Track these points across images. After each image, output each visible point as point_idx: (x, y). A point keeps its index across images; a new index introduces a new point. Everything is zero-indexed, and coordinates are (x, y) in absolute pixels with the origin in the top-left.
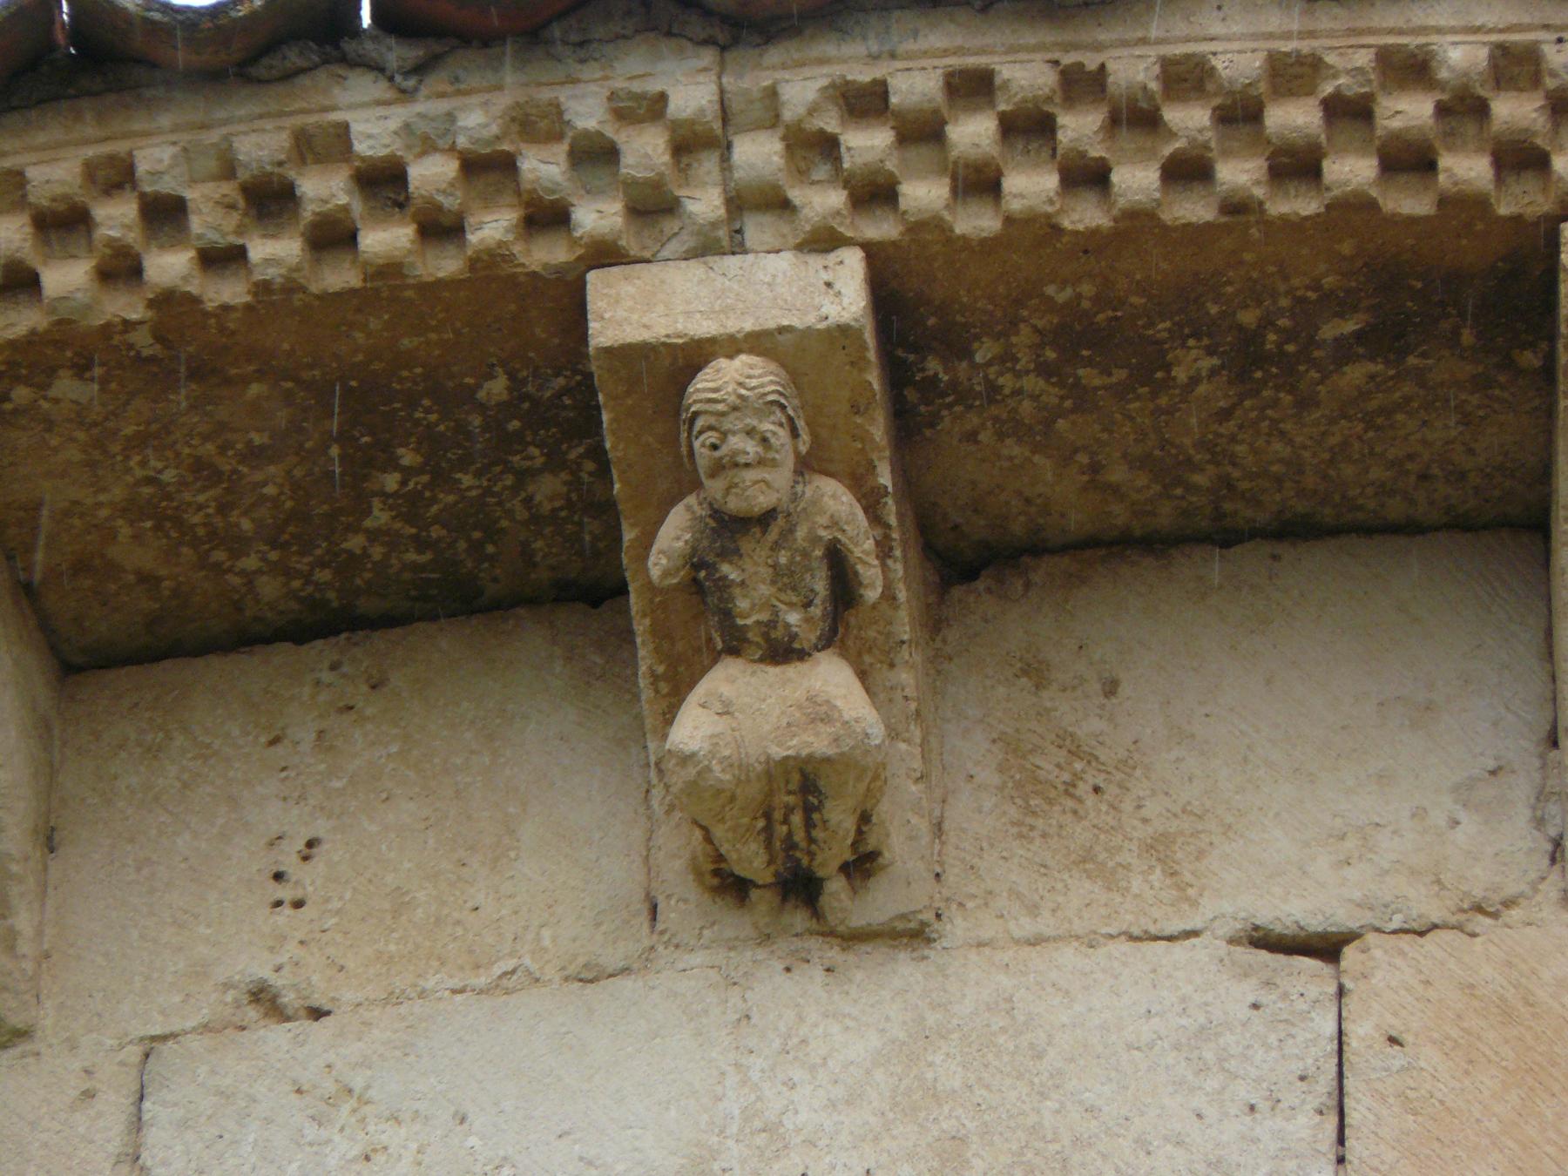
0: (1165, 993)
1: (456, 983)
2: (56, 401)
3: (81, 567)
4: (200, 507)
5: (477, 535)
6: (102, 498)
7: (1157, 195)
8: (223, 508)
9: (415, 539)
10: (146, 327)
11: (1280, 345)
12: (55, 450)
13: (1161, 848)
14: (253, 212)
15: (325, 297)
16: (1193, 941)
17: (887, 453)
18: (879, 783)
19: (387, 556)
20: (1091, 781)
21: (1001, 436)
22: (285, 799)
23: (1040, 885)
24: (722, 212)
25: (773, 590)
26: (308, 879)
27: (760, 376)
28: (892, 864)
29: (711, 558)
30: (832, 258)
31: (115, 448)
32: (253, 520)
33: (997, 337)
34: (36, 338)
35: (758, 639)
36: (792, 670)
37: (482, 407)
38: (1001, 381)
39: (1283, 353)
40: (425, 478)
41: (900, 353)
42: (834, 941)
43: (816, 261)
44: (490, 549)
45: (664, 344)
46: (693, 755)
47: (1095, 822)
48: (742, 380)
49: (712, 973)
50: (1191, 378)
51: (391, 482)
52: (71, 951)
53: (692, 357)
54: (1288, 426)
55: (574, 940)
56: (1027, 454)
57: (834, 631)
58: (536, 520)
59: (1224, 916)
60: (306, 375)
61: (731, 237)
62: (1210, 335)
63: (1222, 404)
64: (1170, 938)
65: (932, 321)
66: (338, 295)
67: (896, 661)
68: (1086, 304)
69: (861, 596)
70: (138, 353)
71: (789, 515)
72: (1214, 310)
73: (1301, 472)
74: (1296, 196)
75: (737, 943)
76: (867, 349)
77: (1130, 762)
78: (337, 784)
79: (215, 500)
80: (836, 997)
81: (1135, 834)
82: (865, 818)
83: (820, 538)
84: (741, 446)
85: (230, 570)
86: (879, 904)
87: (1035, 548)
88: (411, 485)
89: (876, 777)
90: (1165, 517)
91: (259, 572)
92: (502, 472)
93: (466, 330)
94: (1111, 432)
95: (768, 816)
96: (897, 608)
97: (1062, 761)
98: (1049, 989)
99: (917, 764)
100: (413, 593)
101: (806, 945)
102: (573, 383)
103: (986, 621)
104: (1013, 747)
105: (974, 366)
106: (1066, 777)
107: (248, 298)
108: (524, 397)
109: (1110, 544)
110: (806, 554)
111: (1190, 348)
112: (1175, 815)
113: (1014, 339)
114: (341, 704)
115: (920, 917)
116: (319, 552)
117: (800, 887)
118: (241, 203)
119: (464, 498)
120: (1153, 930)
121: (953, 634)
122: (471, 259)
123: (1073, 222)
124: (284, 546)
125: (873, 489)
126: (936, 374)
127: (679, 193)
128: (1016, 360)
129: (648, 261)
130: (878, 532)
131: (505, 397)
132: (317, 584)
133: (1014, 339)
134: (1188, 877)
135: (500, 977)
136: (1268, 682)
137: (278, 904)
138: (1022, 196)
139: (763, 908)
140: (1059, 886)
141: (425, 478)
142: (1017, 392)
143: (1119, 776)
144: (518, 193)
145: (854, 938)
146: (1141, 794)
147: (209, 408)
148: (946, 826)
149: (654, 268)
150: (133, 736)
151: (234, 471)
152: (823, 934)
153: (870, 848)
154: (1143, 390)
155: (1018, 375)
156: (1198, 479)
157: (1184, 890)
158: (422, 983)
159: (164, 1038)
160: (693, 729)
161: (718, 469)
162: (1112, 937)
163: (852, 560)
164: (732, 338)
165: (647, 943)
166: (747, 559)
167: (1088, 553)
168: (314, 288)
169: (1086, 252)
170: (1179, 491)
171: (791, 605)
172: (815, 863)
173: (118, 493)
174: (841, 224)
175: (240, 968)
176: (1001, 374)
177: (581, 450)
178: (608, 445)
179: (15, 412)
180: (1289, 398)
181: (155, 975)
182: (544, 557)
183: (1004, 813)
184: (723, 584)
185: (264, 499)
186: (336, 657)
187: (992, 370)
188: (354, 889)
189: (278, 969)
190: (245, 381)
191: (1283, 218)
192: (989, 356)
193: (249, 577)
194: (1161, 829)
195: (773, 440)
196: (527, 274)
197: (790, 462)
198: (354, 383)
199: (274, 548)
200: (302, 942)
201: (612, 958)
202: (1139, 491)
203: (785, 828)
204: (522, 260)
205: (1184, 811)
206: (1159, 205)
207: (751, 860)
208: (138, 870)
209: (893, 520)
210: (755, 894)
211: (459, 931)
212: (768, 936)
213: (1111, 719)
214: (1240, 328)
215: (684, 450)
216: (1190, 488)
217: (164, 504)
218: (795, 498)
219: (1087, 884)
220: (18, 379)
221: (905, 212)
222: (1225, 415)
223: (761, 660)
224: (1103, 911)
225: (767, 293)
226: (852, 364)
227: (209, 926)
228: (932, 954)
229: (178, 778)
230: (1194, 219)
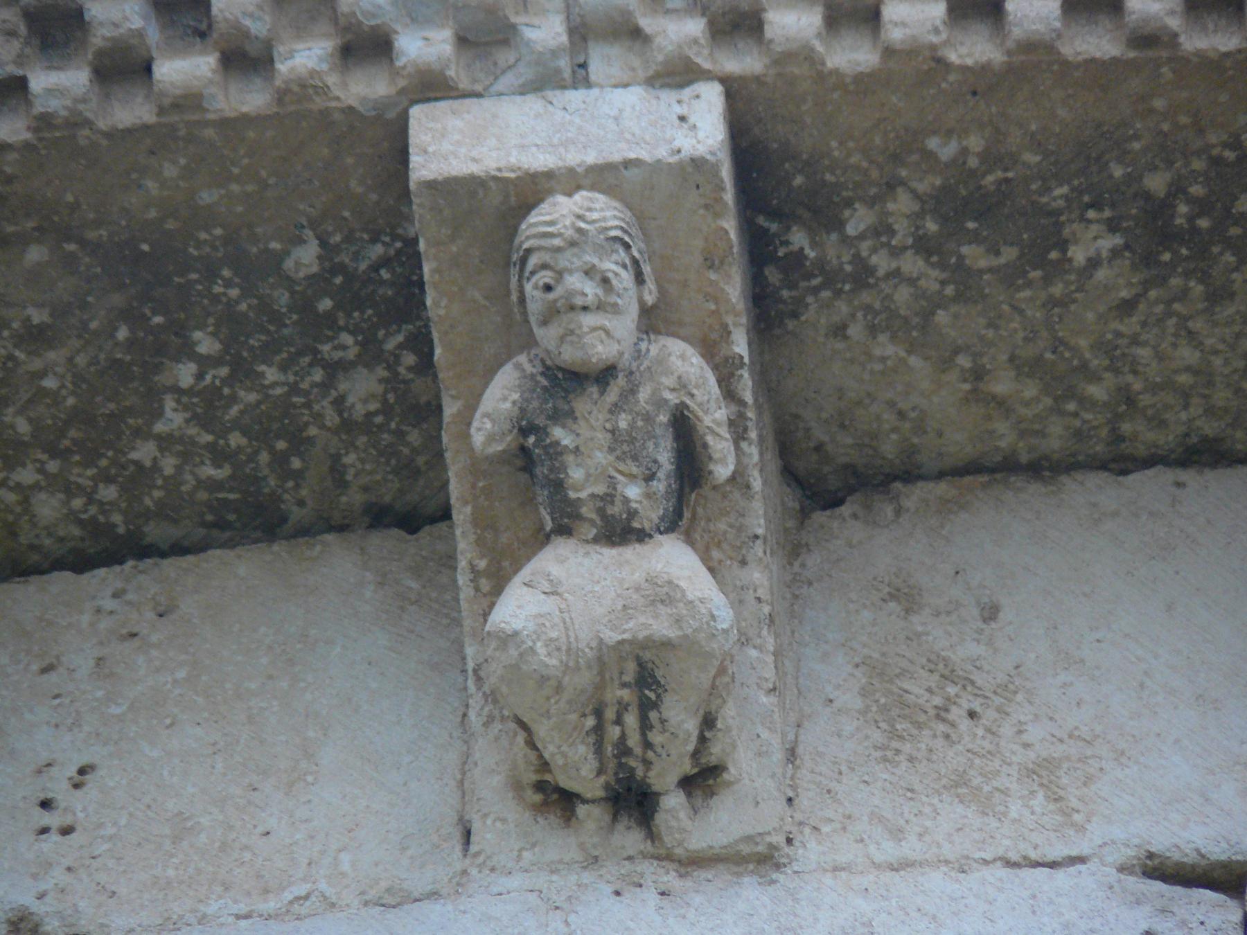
0: (1045, 919)
1: (242, 908)
5: (281, 445)
7: (1058, 24)
9: (211, 447)
11: (1191, 219)
13: (1044, 773)
14: (36, 42)
15: (111, 135)
16: (1082, 867)
17: (744, 320)
18: (727, 679)
19: (179, 469)
20: (966, 705)
21: (873, 330)
22: (57, 726)
23: (906, 811)
24: (564, 39)
25: (611, 458)
26: (78, 806)
27: (602, 210)
28: (738, 781)
29: (540, 421)
30: (687, 92)
32: (30, 420)
33: (872, 202)
35: (593, 516)
36: (630, 552)
37: (289, 282)
38: (874, 259)
39: (1194, 230)
40: (224, 371)
41: (761, 220)
42: (672, 866)
43: (668, 96)
44: (296, 463)
45: (495, 178)
46: (516, 634)
47: (970, 746)
48: (581, 212)
49: (532, 897)
50: (1089, 260)
51: (185, 374)
53: (528, 191)
54: (1197, 325)
55: (376, 865)
56: (902, 354)
57: (678, 513)
58: (348, 426)
59: (1114, 842)
60: (91, 235)
61: (574, 72)
62: (1113, 206)
63: (1124, 294)
64: (1053, 865)
65: (799, 180)
66: (129, 131)
67: (749, 558)
68: (973, 162)
69: (710, 472)
71: (631, 373)
72: (1118, 172)
73: (1210, 384)
74: (1215, 31)
75: (561, 867)
76: (723, 189)
77: (1011, 687)
80: (671, 921)
81: (1014, 759)
82: (708, 722)
83: (666, 401)
84: (578, 286)
86: (720, 824)
87: (908, 473)
88: (208, 378)
89: (722, 671)
90: (1055, 439)
91: (36, 487)
92: (311, 365)
93: (272, 181)
94: (996, 327)
95: (598, 713)
96: (750, 498)
97: (933, 685)
98: (913, 914)
99: (769, 673)
100: (209, 518)
101: (639, 869)
102: (392, 252)
103: (851, 546)
104: (878, 672)
105: (845, 240)
106: (937, 701)
107: (28, 136)
108: (341, 269)
109: (993, 471)
110: (648, 418)
111: (1089, 221)
112: (1061, 741)
113: (891, 206)
114: (124, 631)
115: (768, 839)
116: (104, 463)
117: (633, 801)
118: (23, 29)
119: (267, 396)
120: (1033, 855)
121: (813, 560)
122: (278, 91)
123: (960, 56)
124: (64, 455)
125: (726, 359)
126: (802, 249)
127: (514, 19)
128: (891, 232)
129: (478, 95)
130: (734, 408)
131: (315, 269)
132: (101, 503)
133: (891, 206)
134: (1074, 803)
135: (291, 902)
136: (1170, 608)
137: (44, 831)
138: (904, 24)
139: (591, 825)
140: (927, 810)
141: (224, 371)
142: (896, 274)
143: (998, 700)
144: (335, 20)
145: (693, 862)
146: (1022, 718)
148: (800, 750)
149: (486, 103)
152: (658, 858)
153: (713, 760)
154: (1036, 274)
155: (896, 252)
156: (1096, 391)
157: (1069, 816)
158: (202, 908)
160: (518, 608)
161: (551, 314)
162: (986, 862)
163: (701, 429)
164: (571, 171)
165: (458, 866)
166: (582, 422)
167: (968, 479)
168: (102, 124)
169: (974, 93)
170: (1071, 407)
171: (632, 477)
172: (651, 774)
174: (698, 54)
176: (874, 250)
177: (400, 338)
178: (429, 302)
180: (1200, 288)
182: (356, 475)
183: (867, 737)
184: (555, 452)
185: (45, 392)
186: (119, 585)
187: (865, 246)
188: (131, 815)
189: (41, 896)
190: (23, 240)
191: (1199, 53)
192: (862, 227)
194: (1044, 754)
195: (614, 282)
196: (343, 110)
197: (634, 311)
198: (145, 247)
199: (52, 457)
200: (69, 869)
201: (419, 882)
202: (1027, 404)
203: (617, 729)
204: (338, 93)
205: (1071, 736)
206: (1059, 36)
207: (580, 768)
209: (748, 397)
210: (582, 810)
211: (247, 856)
212: (596, 858)
213: (990, 643)
214: (1148, 196)
215: (514, 297)
216: (1086, 402)
218: (638, 355)
219: (960, 809)
221: (771, 41)
222: (1126, 307)
223: (596, 540)
224: (976, 836)
225: (611, 125)
226: (706, 207)
228: (781, 877)
230: (1098, 55)
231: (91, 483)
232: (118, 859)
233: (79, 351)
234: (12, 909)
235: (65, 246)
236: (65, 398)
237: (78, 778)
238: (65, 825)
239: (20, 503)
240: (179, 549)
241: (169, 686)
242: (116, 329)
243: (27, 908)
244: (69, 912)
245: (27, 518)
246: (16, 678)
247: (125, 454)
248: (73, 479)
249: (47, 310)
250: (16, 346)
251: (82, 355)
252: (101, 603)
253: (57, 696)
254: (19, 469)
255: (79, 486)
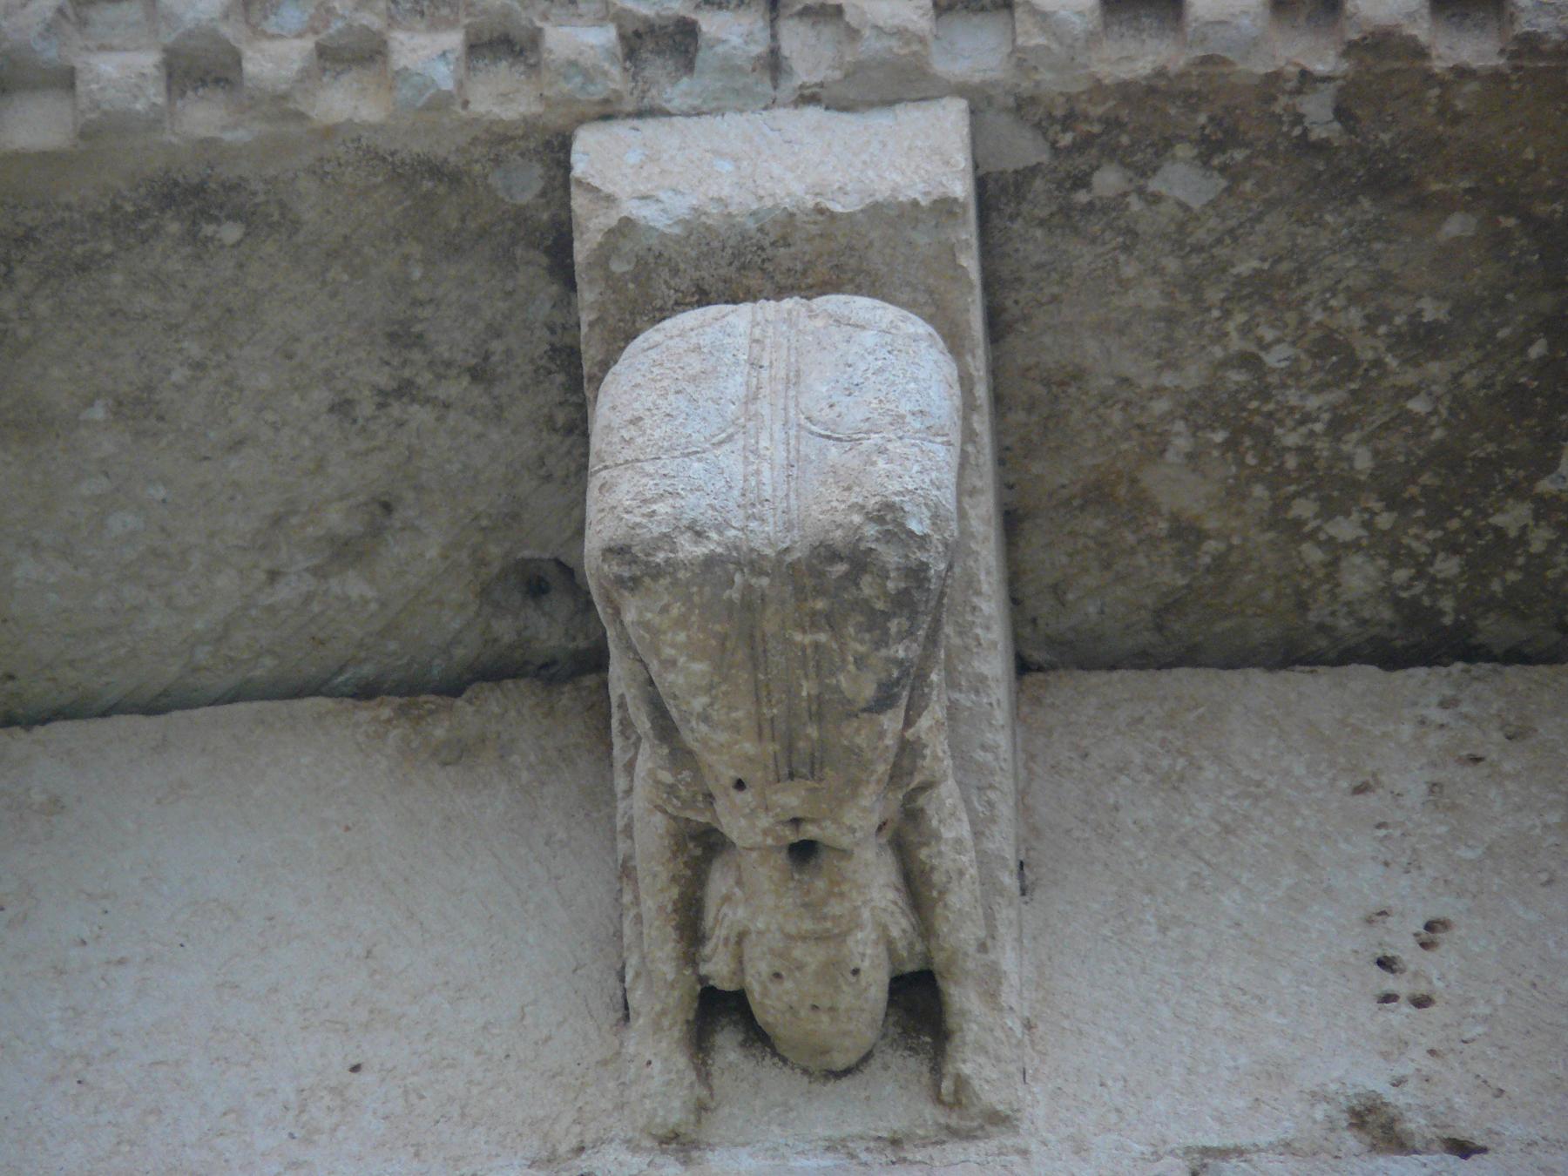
2: (1156, 199)
3: (1097, 495)
4: (1306, 419)
6: (1168, 379)
8: (1339, 425)
10: (1329, 91)
12: (1125, 285)
22: (1386, 864)
26: (1434, 970)
31: (1214, 295)
32: (1376, 453)
34: (1162, 83)
52: (1066, 1024)
60: (1541, 209)
70: (1306, 131)
78: (1465, 853)
79: (1333, 408)
85: (1312, 536)
91: (1355, 545)
114: (1464, 753)
116: (1455, 524)
132: (1434, 580)
137: (1388, 998)
147: (1377, 246)
150: (1138, 759)
151: (1378, 363)
159: (1223, 1153)
173: (1192, 376)
175: (1335, 1074)
179: (1090, 208)
181: (1203, 1069)
185: (1410, 418)
186: (1449, 692)
188: (1509, 992)
190: (1447, 203)
193: (1336, 551)
200: (1432, 1052)
208: (1163, 930)
217: (1254, 404)
220: (1111, 152)
227: (1282, 1014)
229: (1213, 819)
231: (1428, 551)
232: (1501, 1048)
233: (1472, 366)
234: (1357, 1095)
235: (1501, 219)
236: (1433, 428)
237: (1425, 936)
238: (1418, 994)
239: (1325, 565)
240: (1516, 656)
241: (1538, 831)
242: (1531, 343)
243: (1379, 1096)
244: (1442, 1108)
245: (1327, 587)
246: (1320, 795)
247: (1487, 516)
248: (1406, 541)
249: (1447, 305)
250: (1389, 349)
251: (1474, 372)
252: (1425, 712)
253: (1380, 826)
254: (1340, 518)
255: (1411, 553)
